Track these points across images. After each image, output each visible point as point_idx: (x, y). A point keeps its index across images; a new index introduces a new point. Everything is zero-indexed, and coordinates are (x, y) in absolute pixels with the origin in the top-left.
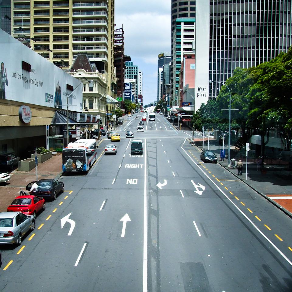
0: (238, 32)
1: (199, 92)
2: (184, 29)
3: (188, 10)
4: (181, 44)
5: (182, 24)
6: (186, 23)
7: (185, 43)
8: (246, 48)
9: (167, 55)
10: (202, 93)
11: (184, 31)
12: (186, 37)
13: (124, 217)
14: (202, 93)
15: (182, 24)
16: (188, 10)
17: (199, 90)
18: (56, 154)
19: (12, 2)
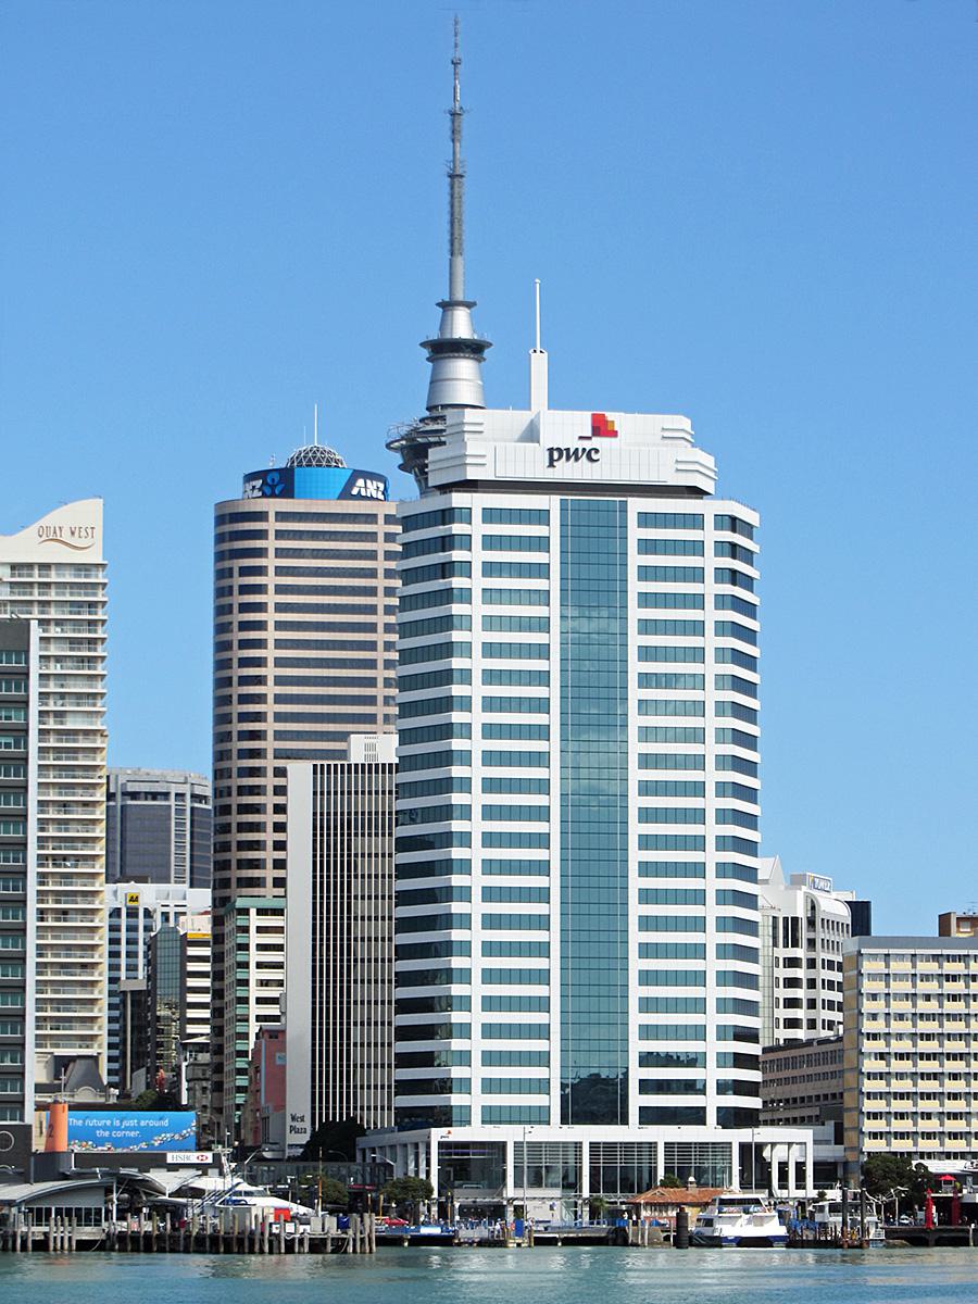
0: (369, 909)
1: (293, 1124)
2: (258, 945)
3: (266, 666)
4: (248, 1003)
5: (253, 912)
6: (261, 912)
7: (260, 1001)
8: (383, 918)
9: (131, 788)
10: (298, 1125)
11: (257, 1003)
12: (262, 947)
13: (740, 828)
14: (298, 1125)
15: (253, 912)
16: (266, 666)
17: (293, 1118)
18: (117, 1057)
19: (2, 778)
